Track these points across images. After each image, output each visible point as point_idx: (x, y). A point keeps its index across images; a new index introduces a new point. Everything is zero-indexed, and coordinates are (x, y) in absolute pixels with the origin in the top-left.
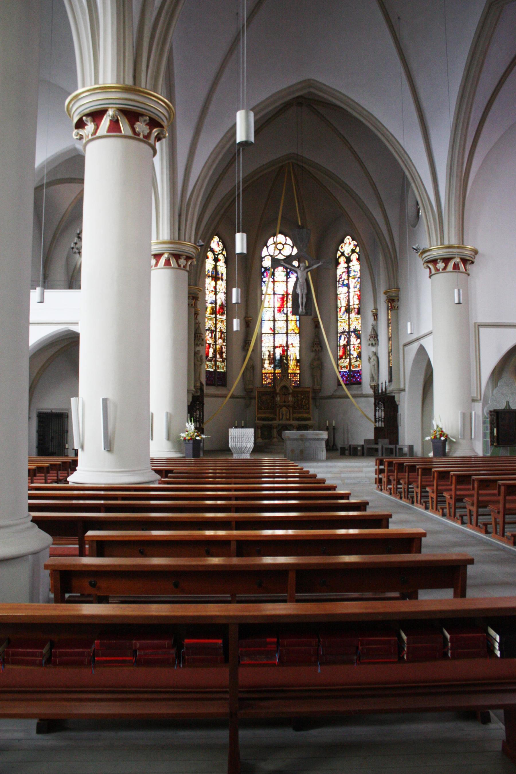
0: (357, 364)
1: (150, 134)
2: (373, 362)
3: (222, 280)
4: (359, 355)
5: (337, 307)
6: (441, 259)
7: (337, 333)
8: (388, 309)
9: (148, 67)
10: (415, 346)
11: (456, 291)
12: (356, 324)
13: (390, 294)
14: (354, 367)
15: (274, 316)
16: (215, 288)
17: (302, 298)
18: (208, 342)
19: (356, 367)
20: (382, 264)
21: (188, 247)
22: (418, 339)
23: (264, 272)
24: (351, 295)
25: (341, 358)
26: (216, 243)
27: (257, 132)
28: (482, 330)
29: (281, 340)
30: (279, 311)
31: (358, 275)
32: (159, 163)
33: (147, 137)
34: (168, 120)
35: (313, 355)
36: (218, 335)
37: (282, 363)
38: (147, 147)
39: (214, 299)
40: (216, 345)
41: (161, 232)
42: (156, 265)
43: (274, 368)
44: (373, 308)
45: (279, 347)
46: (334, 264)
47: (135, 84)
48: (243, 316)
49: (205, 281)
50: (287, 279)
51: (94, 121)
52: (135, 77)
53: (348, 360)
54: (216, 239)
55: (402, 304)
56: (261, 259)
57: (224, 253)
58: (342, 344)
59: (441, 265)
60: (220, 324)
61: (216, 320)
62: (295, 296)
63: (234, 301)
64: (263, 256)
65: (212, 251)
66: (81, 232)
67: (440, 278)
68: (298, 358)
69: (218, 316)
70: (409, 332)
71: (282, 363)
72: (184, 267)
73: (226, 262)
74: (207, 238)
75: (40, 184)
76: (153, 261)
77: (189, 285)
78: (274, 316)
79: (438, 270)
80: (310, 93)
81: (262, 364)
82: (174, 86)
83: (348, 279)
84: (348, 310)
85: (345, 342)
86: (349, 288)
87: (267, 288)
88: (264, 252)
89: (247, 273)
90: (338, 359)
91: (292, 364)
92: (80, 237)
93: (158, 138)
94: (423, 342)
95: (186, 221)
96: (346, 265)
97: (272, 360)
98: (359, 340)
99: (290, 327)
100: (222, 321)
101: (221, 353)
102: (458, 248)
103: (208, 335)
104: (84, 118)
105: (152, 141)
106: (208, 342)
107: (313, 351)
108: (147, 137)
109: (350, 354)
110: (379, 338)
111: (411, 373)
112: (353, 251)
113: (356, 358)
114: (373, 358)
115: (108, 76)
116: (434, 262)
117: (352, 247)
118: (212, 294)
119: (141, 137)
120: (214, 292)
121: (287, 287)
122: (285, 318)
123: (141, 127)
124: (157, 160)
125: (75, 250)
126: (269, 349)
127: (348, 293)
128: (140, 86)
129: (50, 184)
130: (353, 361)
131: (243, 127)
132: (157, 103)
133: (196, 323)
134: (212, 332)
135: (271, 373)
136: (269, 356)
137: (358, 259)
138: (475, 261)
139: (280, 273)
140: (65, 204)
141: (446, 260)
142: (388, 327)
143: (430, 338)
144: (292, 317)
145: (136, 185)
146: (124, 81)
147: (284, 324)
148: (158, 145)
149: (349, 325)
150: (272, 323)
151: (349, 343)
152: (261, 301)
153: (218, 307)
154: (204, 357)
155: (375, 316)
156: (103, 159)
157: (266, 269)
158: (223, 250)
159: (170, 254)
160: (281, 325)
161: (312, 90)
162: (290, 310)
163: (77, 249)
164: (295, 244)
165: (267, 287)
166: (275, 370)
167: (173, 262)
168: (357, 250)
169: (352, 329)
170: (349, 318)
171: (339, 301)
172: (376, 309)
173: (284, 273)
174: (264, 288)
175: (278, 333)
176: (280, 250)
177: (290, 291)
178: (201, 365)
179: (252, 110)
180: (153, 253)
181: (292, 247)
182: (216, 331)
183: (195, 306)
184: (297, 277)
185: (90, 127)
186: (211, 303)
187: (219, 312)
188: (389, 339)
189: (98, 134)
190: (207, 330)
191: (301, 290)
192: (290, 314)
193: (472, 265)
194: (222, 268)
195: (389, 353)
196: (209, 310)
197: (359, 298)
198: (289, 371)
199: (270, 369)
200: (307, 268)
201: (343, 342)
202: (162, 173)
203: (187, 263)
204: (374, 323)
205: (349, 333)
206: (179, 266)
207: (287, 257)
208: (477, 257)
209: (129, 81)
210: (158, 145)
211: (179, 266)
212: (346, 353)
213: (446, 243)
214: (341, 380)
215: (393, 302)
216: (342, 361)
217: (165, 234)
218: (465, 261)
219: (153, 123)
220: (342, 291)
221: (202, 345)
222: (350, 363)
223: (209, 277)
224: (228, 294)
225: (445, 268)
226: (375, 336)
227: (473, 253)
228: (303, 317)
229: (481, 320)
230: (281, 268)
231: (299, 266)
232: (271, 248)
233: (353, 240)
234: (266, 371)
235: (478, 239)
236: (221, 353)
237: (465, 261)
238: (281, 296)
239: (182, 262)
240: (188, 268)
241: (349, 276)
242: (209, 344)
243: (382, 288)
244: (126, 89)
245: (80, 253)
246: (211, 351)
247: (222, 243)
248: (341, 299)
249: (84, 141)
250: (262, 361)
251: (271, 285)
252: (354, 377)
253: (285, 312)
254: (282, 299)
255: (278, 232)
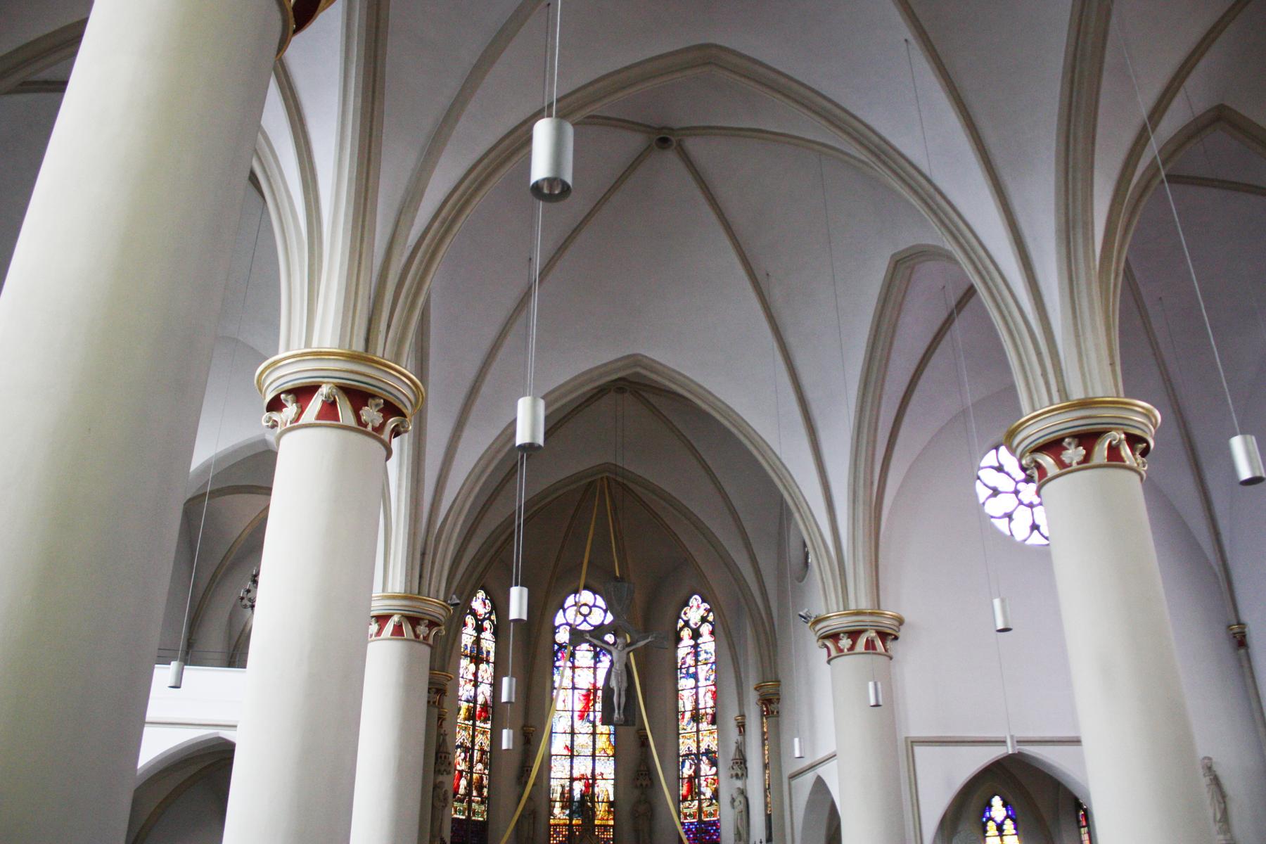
0: (711, 809)
1: (383, 425)
2: (740, 806)
3: (488, 662)
4: (716, 795)
5: (678, 712)
6: (845, 633)
7: (678, 756)
8: (762, 716)
9: (389, 326)
10: (809, 778)
11: (871, 685)
12: (709, 741)
13: (765, 690)
14: (706, 816)
15: (572, 726)
16: (475, 674)
17: (619, 695)
18: (458, 768)
19: (711, 814)
20: (749, 632)
21: (434, 606)
22: (812, 767)
23: (559, 650)
24: (702, 691)
25: (685, 799)
26: (480, 601)
27: (548, 434)
28: (919, 750)
29: (583, 767)
30: (581, 717)
31: (712, 660)
32: (396, 470)
33: (379, 429)
34: (414, 406)
35: (637, 792)
36: (477, 755)
37: (583, 806)
38: (377, 445)
39: (472, 693)
40: (472, 773)
41: (390, 579)
42: (379, 633)
43: (571, 817)
44: (737, 713)
45: (580, 779)
46: (672, 637)
47: (366, 350)
48: (520, 722)
49: (459, 664)
50: (596, 663)
51: (297, 401)
52: (367, 340)
53: (696, 803)
54: (481, 594)
55: (785, 707)
56: (554, 630)
57: (493, 617)
58: (685, 776)
59: (845, 643)
60: (480, 736)
61: (474, 730)
62: (608, 691)
63: (504, 698)
64: (557, 624)
65: (474, 613)
66: (257, 575)
67: (845, 662)
68: (612, 799)
69: (478, 723)
70: (797, 755)
71: (583, 806)
72: (425, 638)
73: (495, 633)
74: (466, 594)
75: (201, 492)
76: (374, 627)
77: (432, 669)
78: (572, 726)
79: (841, 650)
80: (637, 374)
81: (551, 808)
82: (428, 354)
83: (696, 666)
84: (696, 717)
85: (691, 772)
86: (697, 680)
87: (562, 678)
88: (559, 619)
89: (531, 653)
90: (679, 802)
91: (601, 809)
92: (255, 582)
93: (396, 432)
94: (822, 771)
95: (433, 563)
96: (692, 642)
97: (567, 801)
98: (714, 769)
99: (599, 745)
100: (484, 733)
101: (480, 788)
102: (871, 614)
103: (459, 756)
104: (283, 396)
105: (385, 435)
106: (458, 768)
107: (636, 787)
108: (379, 429)
109: (700, 793)
110: (748, 765)
111: (804, 828)
112: (704, 620)
113: (711, 799)
114: (740, 799)
115: (327, 336)
116: (835, 637)
117: (702, 612)
118: (470, 686)
119: (369, 428)
120: (473, 683)
121: (595, 678)
122: (591, 730)
123: (371, 414)
124: (392, 465)
125: (246, 602)
126: (562, 782)
127: (696, 690)
128: (375, 354)
129: (215, 494)
130: (704, 805)
131: (528, 423)
132: (398, 381)
133: (439, 735)
134: (466, 750)
135: (565, 825)
136: (562, 794)
137: (712, 633)
138: (900, 634)
139: (584, 655)
140: (239, 529)
141: (854, 635)
142: (763, 745)
143: (833, 764)
144: (601, 728)
145: (355, 503)
146: (350, 345)
147: (589, 739)
148: (395, 443)
149: (698, 742)
150: (569, 736)
151: (697, 773)
152: (552, 700)
153: (478, 708)
154: (450, 794)
155: (742, 727)
156: (307, 462)
157: (561, 646)
158: (490, 613)
159: (403, 616)
160: (583, 741)
161: (639, 370)
162: (599, 715)
163: (250, 600)
164: (609, 608)
165: (562, 676)
166: (571, 820)
167: (407, 629)
168: (711, 618)
169: (702, 750)
170: (698, 731)
171: (681, 702)
172: (743, 716)
173: (591, 654)
174: (557, 678)
175: (579, 754)
176: (585, 616)
177: (600, 684)
178: (444, 807)
179: (543, 398)
180: (373, 613)
181: (605, 611)
182: (473, 749)
183: (440, 705)
184: (612, 662)
185: (291, 409)
186: (468, 701)
187: (480, 716)
188: (766, 766)
189: (301, 422)
190: (458, 747)
191: (618, 682)
192: (598, 723)
193: (895, 643)
194: (488, 644)
195: (765, 791)
196: (463, 713)
197: (715, 696)
198: (597, 822)
199: (562, 817)
200: (628, 645)
201: (687, 771)
202: (399, 486)
203: (430, 632)
204: (740, 738)
205: (698, 755)
206: (417, 636)
207: (597, 627)
208: (902, 628)
209: (358, 346)
210: (395, 443)
211: (417, 636)
212: (694, 792)
213: (853, 606)
214: (684, 837)
215: (771, 703)
216: (687, 804)
217: (397, 584)
218: (883, 636)
219: (390, 409)
220: (685, 684)
221: (449, 773)
222: (700, 808)
223: (466, 656)
224: (496, 686)
225: (852, 648)
226: (741, 761)
227: (896, 623)
228: (622, 729)
229: (915, 733)
230: (585, 646)
231: (615, 643)
232: (571, 613)
233: (703, 601)
234: (556, 822)
235: (906, 599)
236: (480, 788)
237: (883, 636)
238: (584, 692)
239: (422, 629)
240: (431, 641)
241: (697, 661)
242: (461, 772)
243: (752, 681)
244: (353, 357)
245: (253, 607)
246: (463, 783)
247: (491, 601)
248: (685, 698)
249: (278, 430)
250: (551, 803)
251: (568, 672)
252: (707, 832)
253: (591, 718)
254: (587, 697)
255: (582, 586)
